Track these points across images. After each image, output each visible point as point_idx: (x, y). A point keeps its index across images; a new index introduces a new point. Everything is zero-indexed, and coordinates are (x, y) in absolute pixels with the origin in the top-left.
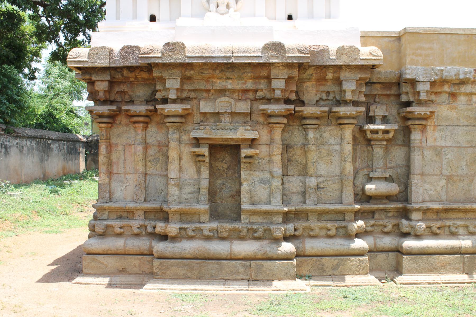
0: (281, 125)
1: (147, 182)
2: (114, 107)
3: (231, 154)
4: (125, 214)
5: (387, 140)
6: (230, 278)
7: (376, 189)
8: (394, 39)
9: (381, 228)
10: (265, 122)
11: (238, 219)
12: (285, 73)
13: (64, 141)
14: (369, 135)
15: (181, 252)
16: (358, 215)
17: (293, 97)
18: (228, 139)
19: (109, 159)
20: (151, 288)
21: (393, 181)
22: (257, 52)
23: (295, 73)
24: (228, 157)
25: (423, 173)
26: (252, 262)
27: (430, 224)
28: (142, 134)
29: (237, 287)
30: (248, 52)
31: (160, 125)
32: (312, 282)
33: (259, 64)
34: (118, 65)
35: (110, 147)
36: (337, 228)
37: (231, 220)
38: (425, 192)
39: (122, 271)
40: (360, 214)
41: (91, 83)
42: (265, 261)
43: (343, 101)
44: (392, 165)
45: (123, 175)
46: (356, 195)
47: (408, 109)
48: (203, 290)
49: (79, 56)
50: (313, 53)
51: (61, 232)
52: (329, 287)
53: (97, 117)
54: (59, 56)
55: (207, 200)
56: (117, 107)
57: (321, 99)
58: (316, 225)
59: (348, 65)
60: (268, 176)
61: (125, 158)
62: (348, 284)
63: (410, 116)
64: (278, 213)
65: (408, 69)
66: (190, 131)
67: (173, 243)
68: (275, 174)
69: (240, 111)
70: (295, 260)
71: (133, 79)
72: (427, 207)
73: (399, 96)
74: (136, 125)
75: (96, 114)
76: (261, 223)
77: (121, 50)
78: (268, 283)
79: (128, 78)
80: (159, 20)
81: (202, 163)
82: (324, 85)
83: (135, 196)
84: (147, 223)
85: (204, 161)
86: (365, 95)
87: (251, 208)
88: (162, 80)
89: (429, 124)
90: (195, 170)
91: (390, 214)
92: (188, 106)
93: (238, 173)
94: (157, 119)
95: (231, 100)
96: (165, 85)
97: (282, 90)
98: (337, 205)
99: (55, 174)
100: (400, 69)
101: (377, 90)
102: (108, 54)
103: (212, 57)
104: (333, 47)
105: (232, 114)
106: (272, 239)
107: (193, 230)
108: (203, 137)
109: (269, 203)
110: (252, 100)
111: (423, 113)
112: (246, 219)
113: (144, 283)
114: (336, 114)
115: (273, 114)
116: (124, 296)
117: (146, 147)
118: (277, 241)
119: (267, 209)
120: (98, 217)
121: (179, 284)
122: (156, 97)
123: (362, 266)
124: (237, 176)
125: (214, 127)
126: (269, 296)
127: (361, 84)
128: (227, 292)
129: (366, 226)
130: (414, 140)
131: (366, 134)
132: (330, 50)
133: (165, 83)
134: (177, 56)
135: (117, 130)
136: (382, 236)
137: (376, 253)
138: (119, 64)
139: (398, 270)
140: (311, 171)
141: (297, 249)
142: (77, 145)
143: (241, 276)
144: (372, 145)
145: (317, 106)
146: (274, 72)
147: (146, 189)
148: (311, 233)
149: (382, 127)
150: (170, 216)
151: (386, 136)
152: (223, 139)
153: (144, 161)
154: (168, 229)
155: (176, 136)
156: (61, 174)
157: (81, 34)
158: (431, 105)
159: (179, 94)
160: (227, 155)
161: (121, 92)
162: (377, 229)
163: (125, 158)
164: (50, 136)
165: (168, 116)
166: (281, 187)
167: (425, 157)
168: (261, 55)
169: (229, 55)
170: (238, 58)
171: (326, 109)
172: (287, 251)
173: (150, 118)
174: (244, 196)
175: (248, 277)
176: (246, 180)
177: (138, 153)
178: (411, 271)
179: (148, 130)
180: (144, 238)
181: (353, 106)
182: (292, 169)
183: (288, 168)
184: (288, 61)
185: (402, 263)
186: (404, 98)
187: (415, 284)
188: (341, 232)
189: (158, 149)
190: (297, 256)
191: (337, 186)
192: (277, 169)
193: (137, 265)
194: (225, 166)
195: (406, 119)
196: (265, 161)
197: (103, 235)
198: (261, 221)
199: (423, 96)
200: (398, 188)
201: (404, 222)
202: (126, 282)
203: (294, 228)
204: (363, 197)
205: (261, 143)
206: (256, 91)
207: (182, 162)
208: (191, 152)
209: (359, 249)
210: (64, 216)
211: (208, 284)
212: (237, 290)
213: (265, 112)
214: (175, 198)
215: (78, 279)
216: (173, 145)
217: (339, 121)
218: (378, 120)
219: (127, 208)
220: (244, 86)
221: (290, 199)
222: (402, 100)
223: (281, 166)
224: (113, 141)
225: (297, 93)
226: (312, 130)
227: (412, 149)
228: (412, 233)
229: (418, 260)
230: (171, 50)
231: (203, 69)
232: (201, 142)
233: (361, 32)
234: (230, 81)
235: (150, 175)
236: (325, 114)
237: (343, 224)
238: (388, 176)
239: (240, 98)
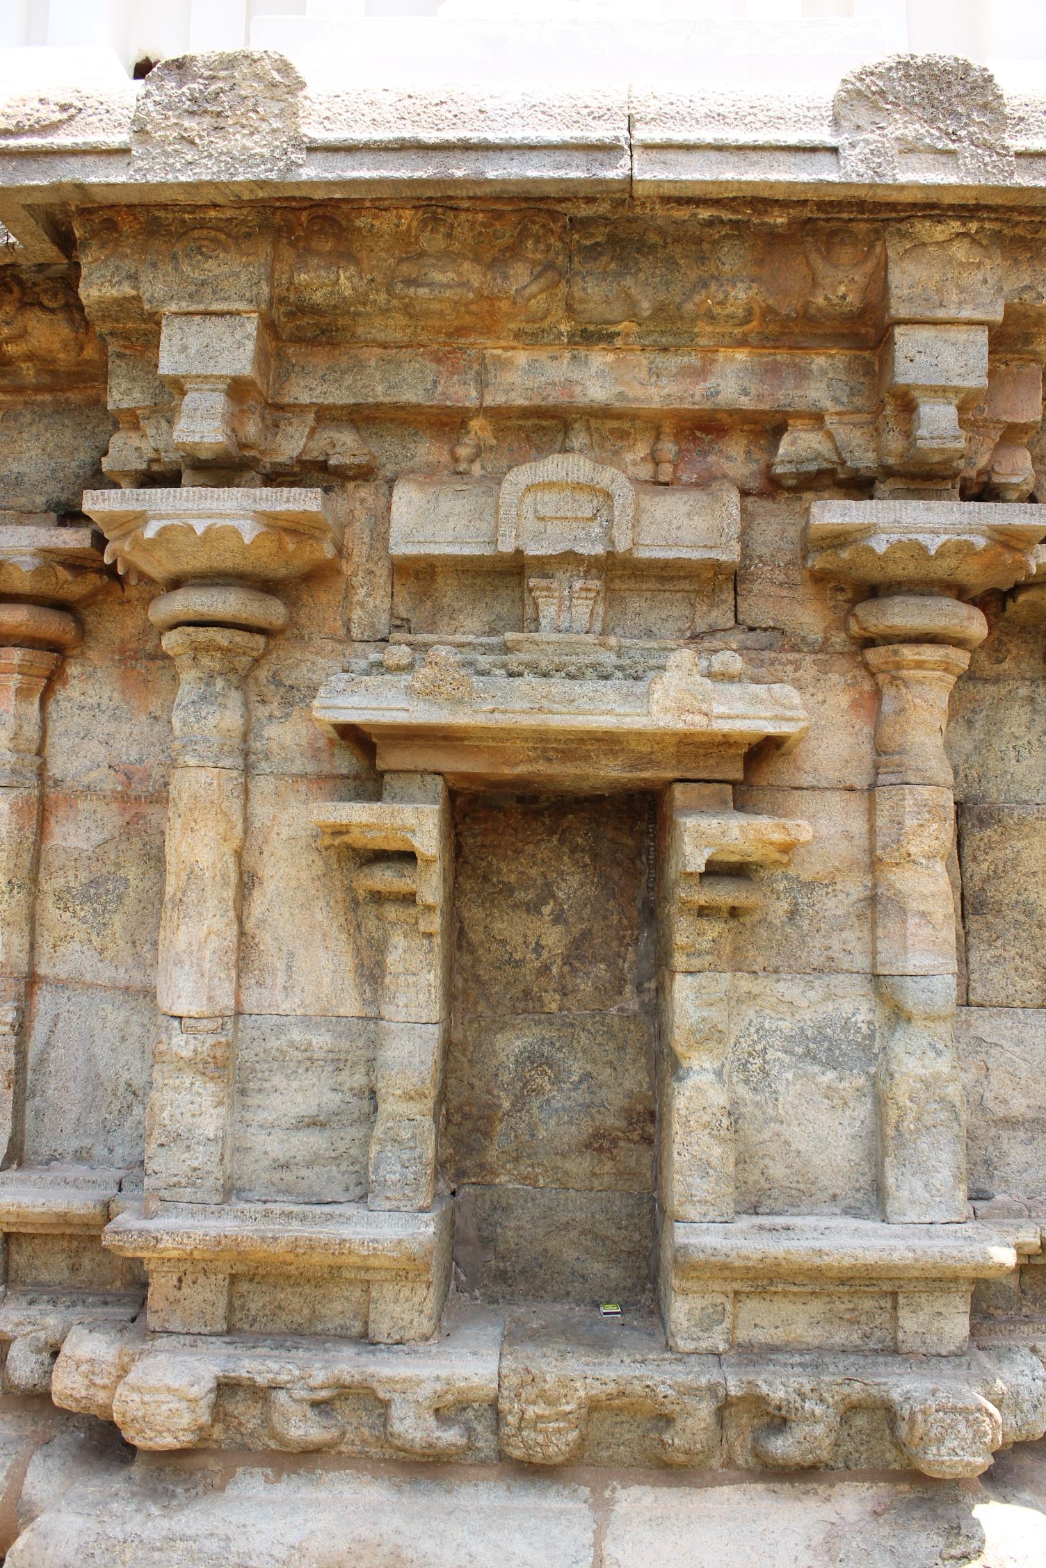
1: (39, 1030)
3: (595, 856)
24: (574, 881)
27: (256, 1366)
28: (18, 717)
30: (740, 119)
31: (141, 667)
60: (857, 1008)
64: (939, 1281)
68: (914, 996)
69: (671, 554)
76: (816, 1357)
81: (392, 912)
85: (409, 899)
88: (142, 334)
90: (348, 961)
94: (115, 626)
105: (619, 574)
107: (315, 1404)
108: (401, 718)
109: (874, 1199)
110: (744, 493)
112: (706, 1324)
119: (871, 1257)
124: (633, 1005)
125: (483, 661)
146: (909, 279)
150: (160, 1287)
153: (20, 896)
159: (251, 429)
160: (566, 864)
168: (832, 142)
169: (600, 133)
170: (671, 156)
176: (710, 1036)
179: (61, 694)
182: (998, 961)
189: (119, 821)
194: (554, 938)
198: (812, 1336)
205: (806, 780)
207: (258, 905)
214: (199, 1157)
216: (199, 782)
220: (699, 389)
231: (422, 254)
232: (389, 759)
234: (599, 359)
235: (61, 984)
239: (666, 472)
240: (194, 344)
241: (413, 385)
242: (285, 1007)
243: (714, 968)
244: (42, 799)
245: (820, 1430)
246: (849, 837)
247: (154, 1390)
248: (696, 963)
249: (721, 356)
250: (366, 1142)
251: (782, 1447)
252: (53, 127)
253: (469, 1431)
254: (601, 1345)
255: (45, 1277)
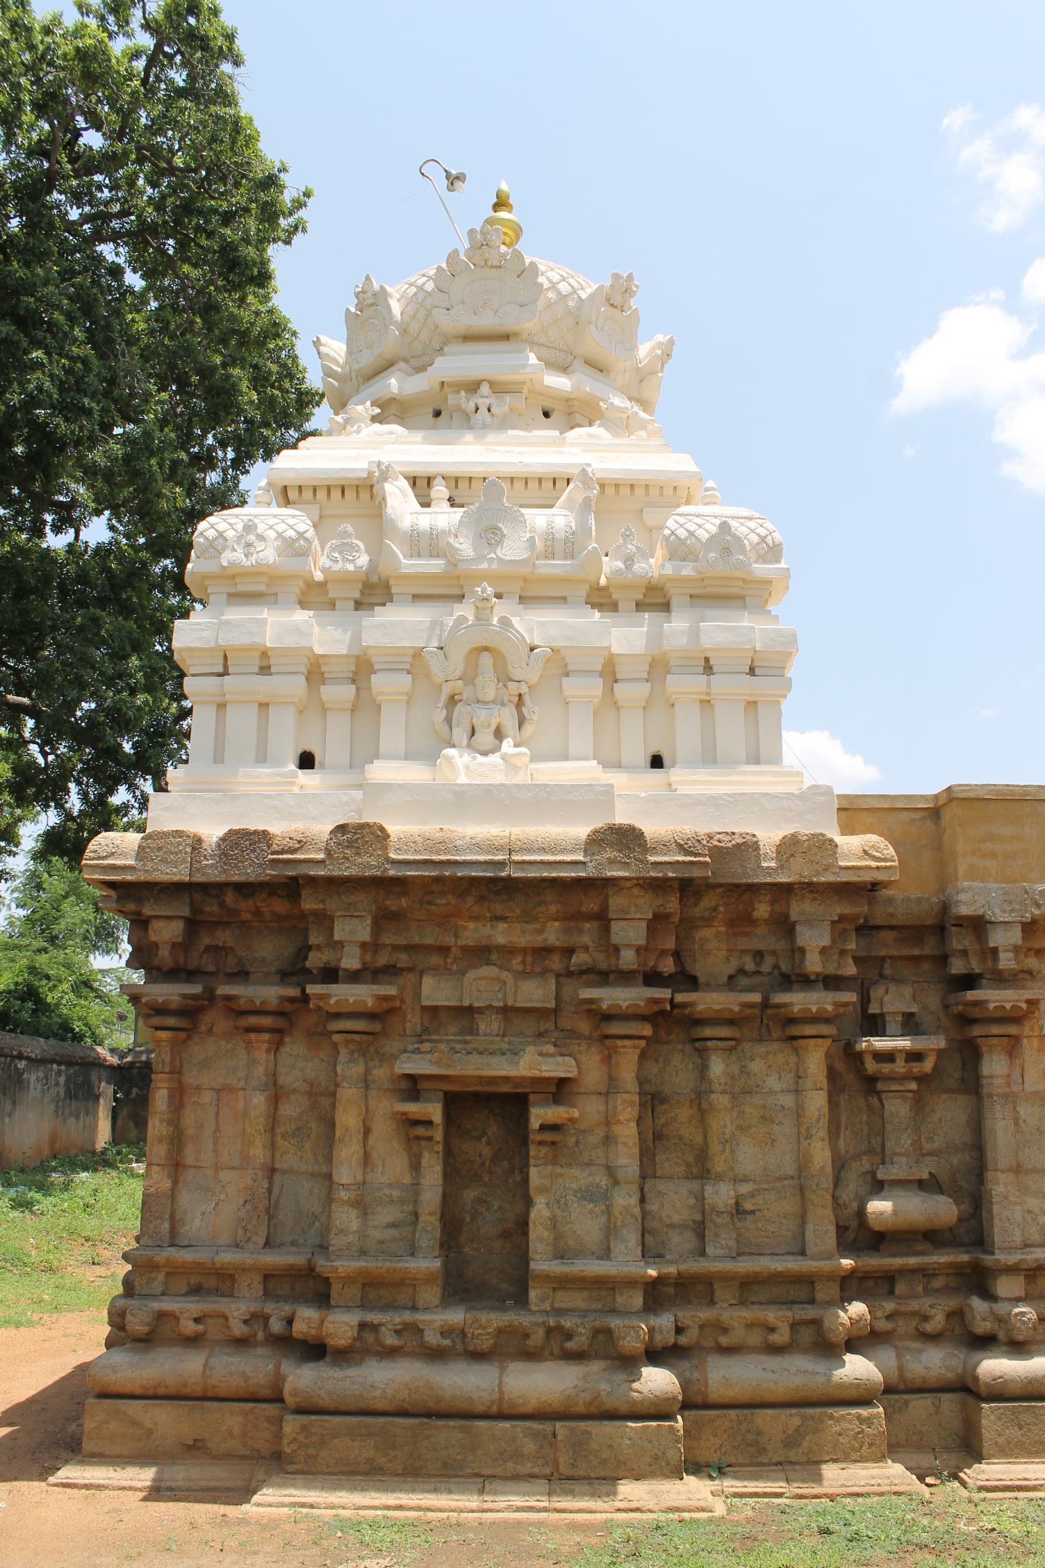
0: (636, 1042)
1: (276, 1191)
2: (197, 989)
4: (211, 1282)
5: (921, 1079)
6: (498, 1471)
7: (895, 1212)
8: (923, 814)
9: (914, 1323)
10: (595, 1035)
11: (521, 1299)
12: (645, 906)
13: (59, 1064)
14: (871, 1066)
15: (361, 1396)
16: (850, 1286)
17: (668, 966)
18: (495, 1078)
19: (176, 1127)
20: (274, 1501)
21: (941, 1191)
22: (573, 851)
23: (672, 904)
25: (1019, 1165)
26: (558, 1425)
27: (374, 1317)
29: (518, 1501)
32: (730, 1485)
33: (578, 881)
34: (213, 879)
35: (179, 1094)
36: (794, 1326)
37: (498, 1300)
38: (1028, 1217)
39: (195, 1448)
40: (854, 1283)
41: (140, 924)
42: (596, 1423)
43: (798, 975)
44: (936, 1145)
45: (210, 1172)
46: (841, 1229)
47: (971, 995)
48: (419, 1509)
49: (113, 854)
50: (720, 854)
51: (30, 1324)
52: (777, 1501)
53: (149, 1011)
54: (63, 845)
55: (437, 1246)
56: (205, 987)
57: (741, 971)
58: (735, 1316)
59: (810, 884)
60: (602, 1180)
61: (217, 1125)
62: (830, 1491)
63: (976, 1013)
64: (630, 1283)
65: (963, 890)
66: (394, 1057)
67: (340, 1366)
68: (620, 1175)
69: (529, 1005)
70: (679, 1417)
71: (250, 916)
72: (1036, 1260)
73: (943, 959)
74: (253, 1036)
75: (146, 1004)
76: (584, 1313)
77: (223, 839)
78: (604, 1489)
79: (236, 912)
80: (323, 766)
81: (424, 1143)
82: (747, 934)
83: (240, 1232)
84: (269, 1308)
85: (430, 1139)
86: (857, 960)
87: (556, 1268)
88: (325, 920)
89: (1026, 1033)
90: (406, 1162)
91: (938, 1283)
92: (390, 990)
93: (521, 1171)
95: (505, 975)
96: (332, 934)
97: (638, 950)
98: (791, 1258)
99: (29, 1153)
100: (942, 890)
101: (887, 946)
102: (189, 850)
103: (456, 862)
104: (769, 836)
105: (507, 1012)
106: (613, 1358)
108: (428, 1072)
109: (606, 1254)
110: (558, 976)
111: (1008, 1006)
112: (543, 1300)
113: (254, 1484)
114: (783, 1010)
115: (614, 1012)
116: (193, 1525)
117: (276, 1094)
118: (628, 1363)
120: (137, 1287)
121: (353, 1489)
122: (308, 964)
123: (868, 1435)
124: (519, 1179)
125: (458, 1047)
126: (608, 1527)
127: (845, 931)
128: (489, 1514)
129: (874, 1317)
130: (991, 1077)
131: (862, 1063)
132: (761, 844)
133: (332, 928)
134: (366, 859)
135: (199, 1050)
136: (917, 1345)
137: (906, 1397)
138: (215, 876)
139: (969, 1447)
140: (719, 1165)
141: (685, 1384)
142: (94, 1076)
143: (528, 1468)
144: (878, 1093)
145: (731, 990)
146: (616, 902)
147: (271, 1213)
148: (724, 1340)
149: (904, 1043)
150: (335, 1289)
151: (916, 1068)
152: (481, 1080)
153: (268, 1135)
154: (329, 1327)
155: (358, 1069)
156: (46, 1153)
157: (122, 789)
158: (1029, 984)
159: (368, 958)
161: (217, 948)
162: (904, 1326)
163: (217, 1125)
164: (23, 1049)
165: (337, 1016)
166: (637, 1211)
167: (1021, 1124)
168: (582, 858)
170: (524, 866)
171: (756, 998)
172: (658, 1393)
173: (290, 1020)
174: (538, 1234)
175: (548, 1470)
176: (543, 1190)
177: (253, 1114)
178: (1010, 1451)
179: (282, 1050)
180: (260, 1351)
181: (827, 988)
182: (668, 1159)
183: (658, 1158)
184: (653, 874)
185: (979, 1427)
186: (957, 967)
187: (1020, 1488)
188: (806, 1335)
190: (686, 1406)
191: (789, 1205)
192: (627, 1160)
193: (236, 1430)
194: (487, 1151)
195: (966, 1021)
196: (593, 1139)
197: (146, 1341)
198: (584, 1305)
199: (1006, 961)
200: (954, 1208)
201: (978, 1305)
202: (203, 1483)
203: (677, 1326)
204: (860, 1235)
205: (583, 1090)
206: (569, 951)
207: (371, 1140)
208: (397, 1113)
209: (858, 1385)
210: (44, 1277)
211: (435, 1490)
212: (519, 1509)
213: (593, 1007)
215: (68, 1473)
216: (348, 1093)
217: (789, 1030)
218: (893, 1024)
219: (218, 1265)
220: (540, 939)
221: (663, 1242)
222: (954, 972)
223: (638, 1152)
224: (190, 1078)
225: (677, 955)
226: (719, 1053)
227: (987, 1102)
228: (1002, 1335)
229: (1026, 1417)
230: (350, 844)
233: (839, 796)
234: (502, 926)
235: (285, 1172)
236: (753, 1011)
237: (810, 1312)
238: (925, 1176)
239: (528, 969)
240: (347, 929)
241: (430, 936)
242: (382, 1180)
243: (544, 1164)
244: (276, 1094)
245: (584, 1338)
246: (599, 1112)
247: (339, 1322)
248: (538, 1162)
249: (549, 924)
250: (414, 1232)
251: (570, 1345)
252: (294, 851)
253: (454, 1342)
254: (504, 1310)
255: (280, 1292)
